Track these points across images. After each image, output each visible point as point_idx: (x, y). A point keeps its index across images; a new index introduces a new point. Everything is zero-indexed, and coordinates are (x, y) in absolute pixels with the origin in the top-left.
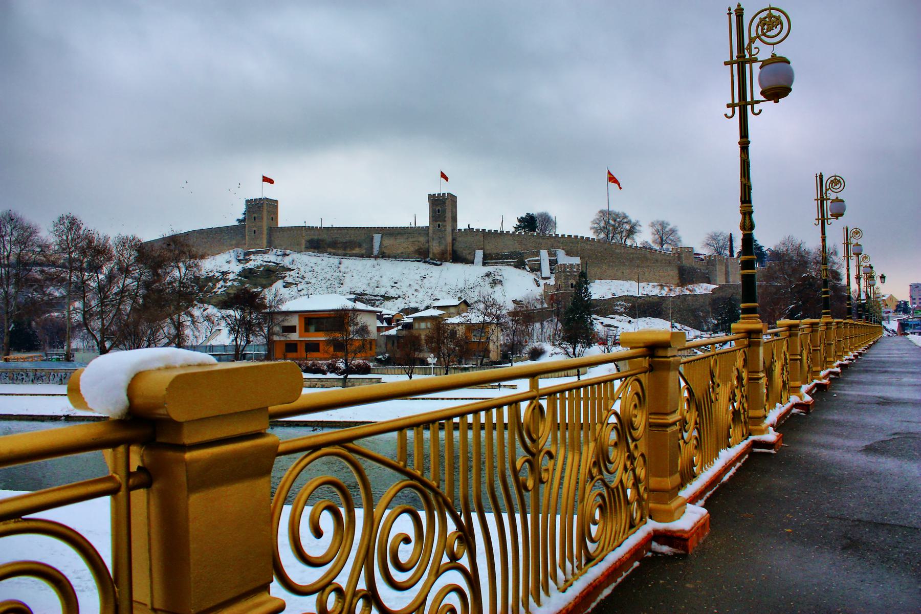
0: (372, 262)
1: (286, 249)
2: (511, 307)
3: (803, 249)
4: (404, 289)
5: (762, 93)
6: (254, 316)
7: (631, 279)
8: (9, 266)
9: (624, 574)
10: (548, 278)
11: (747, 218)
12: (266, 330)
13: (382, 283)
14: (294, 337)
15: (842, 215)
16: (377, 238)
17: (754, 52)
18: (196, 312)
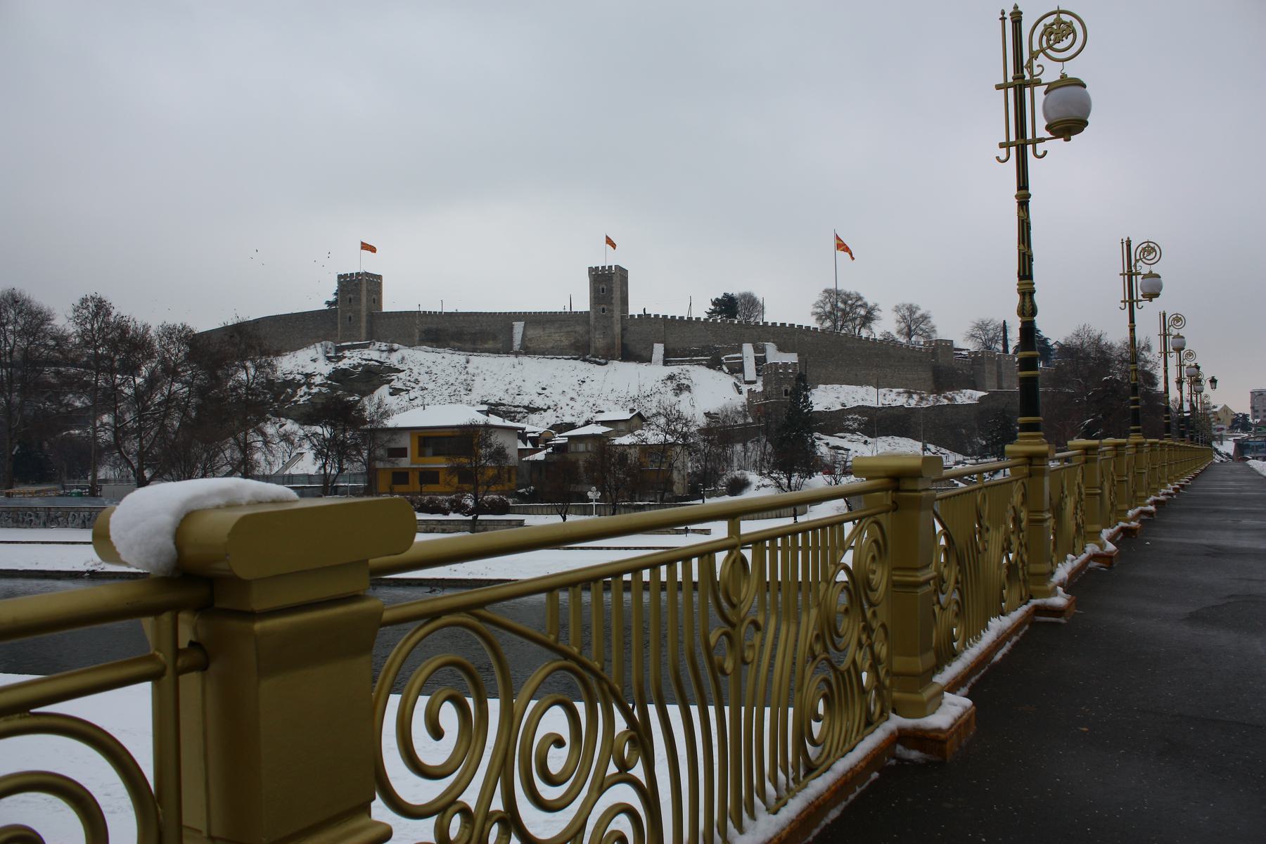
0: (512, 359)
2: (702, 421)
3: (1103, 342)
5: (1048, 128)
7: (868, 384)
8: (12, 365)
9: (858, 790)
10: (754, 382)
11: (1027, 300)
12: (365, 454)
14: (405, 463)
15: (1157, 295)
16: (518, 327)
17: (1036, 71)
18: (270, 429)
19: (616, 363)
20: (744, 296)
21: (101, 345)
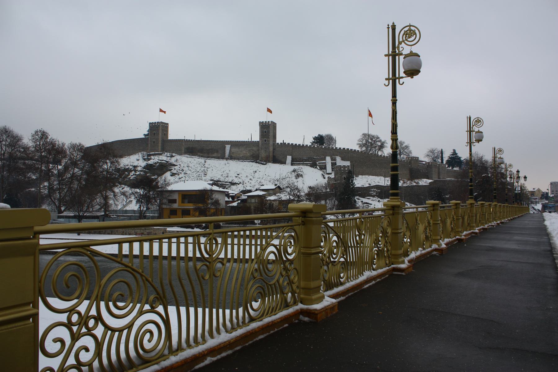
0: (224, 161)
1: (173, 153)
2: (306, 190)
3: (484, 160)
4: (244, 178)
5: (404, 72)
6: (151, 193)
7: (381, 175)
8: (4, 159)
9: (276, 330)
10: (331, 174)
12: (158, 201)
13: (230, 175)
14: (175, 206)
15: (481, 140)
16: (228, 147)
17: (401, 49)
18: (117, 190)
19: (270, 164)
20: (327, 136)
21: (44, 152)
